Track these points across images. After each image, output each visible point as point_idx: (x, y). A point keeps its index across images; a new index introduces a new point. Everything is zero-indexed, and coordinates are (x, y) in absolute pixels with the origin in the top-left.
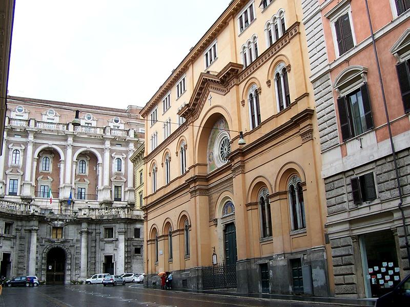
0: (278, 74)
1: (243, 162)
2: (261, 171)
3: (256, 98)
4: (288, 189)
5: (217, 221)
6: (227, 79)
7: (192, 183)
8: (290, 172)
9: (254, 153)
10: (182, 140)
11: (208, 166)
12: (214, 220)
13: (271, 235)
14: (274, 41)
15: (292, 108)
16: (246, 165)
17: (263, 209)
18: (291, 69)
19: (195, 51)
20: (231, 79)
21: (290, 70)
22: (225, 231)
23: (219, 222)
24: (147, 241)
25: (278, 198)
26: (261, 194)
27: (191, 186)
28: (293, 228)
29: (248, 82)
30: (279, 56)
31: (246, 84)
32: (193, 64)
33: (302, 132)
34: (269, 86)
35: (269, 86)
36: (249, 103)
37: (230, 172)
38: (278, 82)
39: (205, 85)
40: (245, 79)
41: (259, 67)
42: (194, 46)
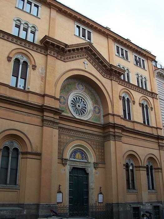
20: (53, 50)
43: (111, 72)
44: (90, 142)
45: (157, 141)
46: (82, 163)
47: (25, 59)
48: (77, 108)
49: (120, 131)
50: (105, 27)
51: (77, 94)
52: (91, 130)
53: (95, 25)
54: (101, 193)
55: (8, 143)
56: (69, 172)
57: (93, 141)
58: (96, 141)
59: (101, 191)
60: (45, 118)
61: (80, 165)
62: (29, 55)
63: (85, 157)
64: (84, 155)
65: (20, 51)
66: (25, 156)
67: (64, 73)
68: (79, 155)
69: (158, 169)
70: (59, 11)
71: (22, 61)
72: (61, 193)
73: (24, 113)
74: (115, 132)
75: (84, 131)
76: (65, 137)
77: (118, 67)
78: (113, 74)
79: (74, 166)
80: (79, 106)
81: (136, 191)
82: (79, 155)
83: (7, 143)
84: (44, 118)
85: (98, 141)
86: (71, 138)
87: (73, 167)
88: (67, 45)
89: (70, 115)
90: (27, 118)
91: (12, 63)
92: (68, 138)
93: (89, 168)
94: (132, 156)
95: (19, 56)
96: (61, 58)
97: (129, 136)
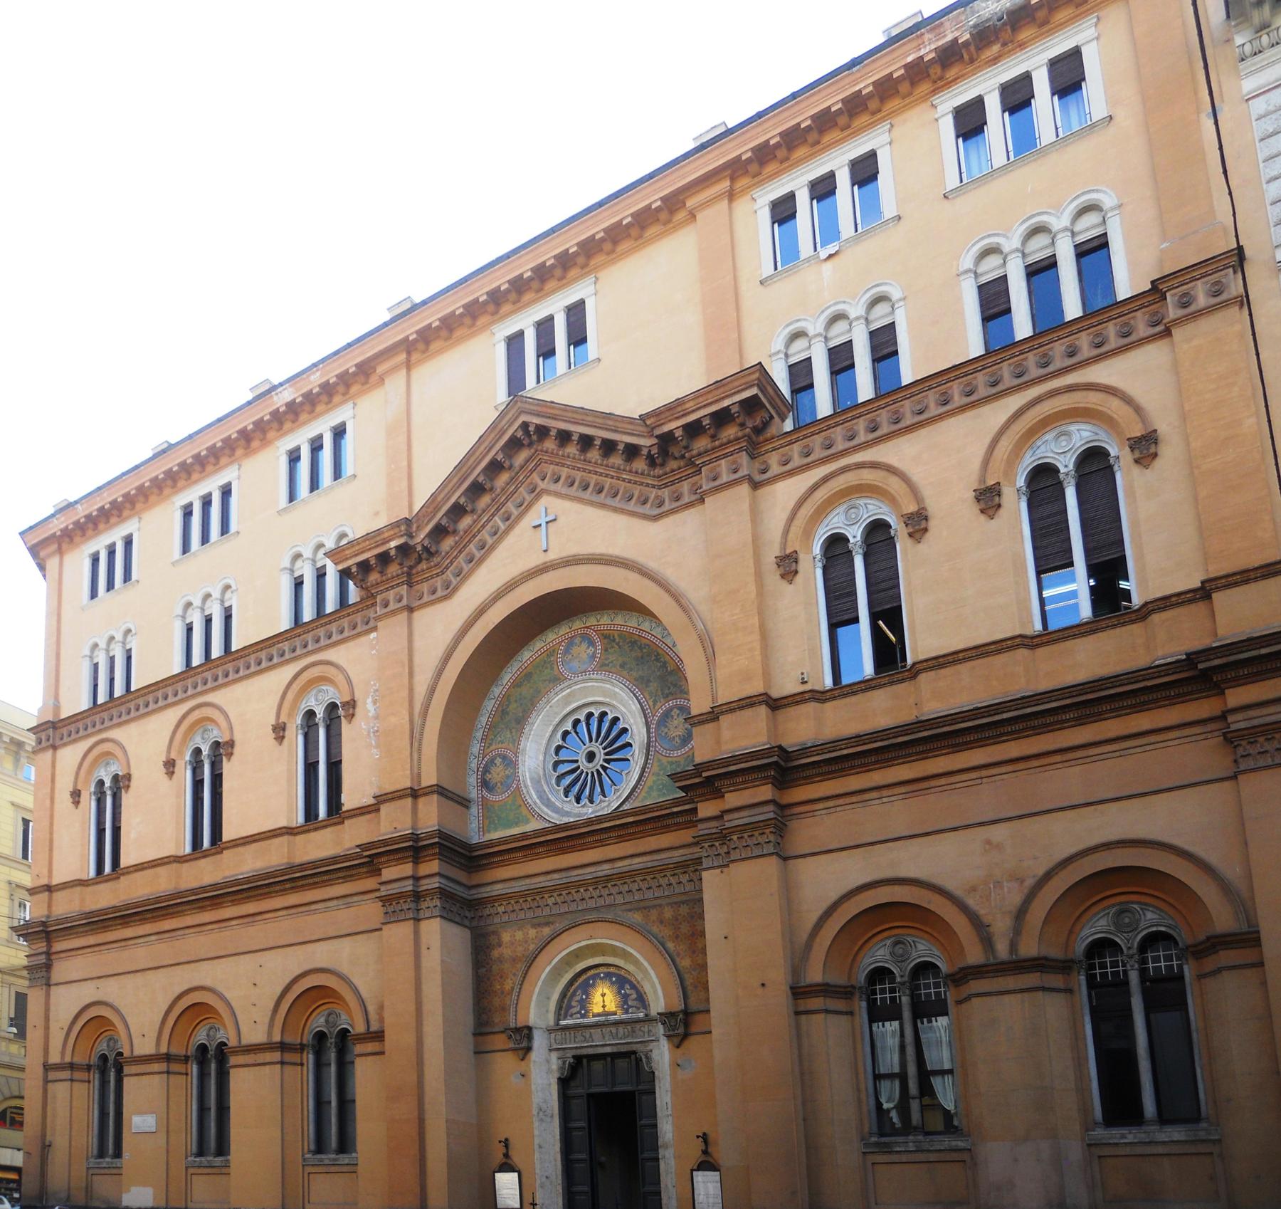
0: (310, 714)
1: (784, 810)
2: (110, 991)
3: (328, 728)
4: (94, 1060)
5: (530, 1037)
6: (702, 443)
7: (401, 861)
8: (313, 994)
9: (877, 777)
10: (108, 754)
11: (474, 810)
12: (517, 1030)
13: (118, 1154)
14: (101, 699)
15: (346, 822)
16: (793, 824)
17: (203, 1076)
18: (176, 770)
19: (172, 463)
20: (717, 453)
21: (353, 715)
22: (564, 1083)
23: (539, 1041)
24: (47, 1067)
25: (1032, 979)
26: (201, 1037)
27: (389, 873)
28: (195, 1149)
29: (826, 479)
30: (874, 465)
31: (184, 717)
32: (409, 366)
33: (385, 891)
34: (171, 774)
35: (171, 774)
36: (94, 804)
37: (685, 836)
38: (306, 736)
39: (531, 447)
40: (193, 696)
41: (126, 722)
42: (72, 500)
43: (683, 457)
44: (637, 917)
45: (370, 883)
46: (614, 1030)
47: (1082, 435)
48: (605, 761)
49: (407, 869)
50: (881, 39)
51: (568, 703)
52: (632, 856)
53: (861, 79)
54: (707, 1165)
55: (881, 952)
56: (559, 1079)
57: (655, 906)
58: (668, 901)
59: (705, 1152)
60: (1238, 722)
61: (603, 1043)
62: (1093, 399)
63: (634, 996)
64: (633, 987)
65: (821, 494)
66: (1210, 963)
67: (77, 774)
68: (603, 995)
69: (1217, 943)
70: (743, 182)
71: (1066, 465)
72: (514, 1171)
73: (335, 902)
74: (416, 879)
75: (605, 869)
76: (519, 935)
77: (344, 541)
78: (699, 454)
79: (579, 1052)
80: (591, 757)
81: (961, 1144)
82: (603, 995)
83: (1097, 926)
84: (1233, 727)
85: (668, 901)
86: (547, 931)
87: (574, 1057)
88: (407, 521)
89: (534, 825)
90: (345, 917)
91: (1017, 509)
92: (532, 932)
93: (651, 1046)
94: (194, 1010)
95: (836, 522)
96: (1185, 305)
97: (260, 913)
